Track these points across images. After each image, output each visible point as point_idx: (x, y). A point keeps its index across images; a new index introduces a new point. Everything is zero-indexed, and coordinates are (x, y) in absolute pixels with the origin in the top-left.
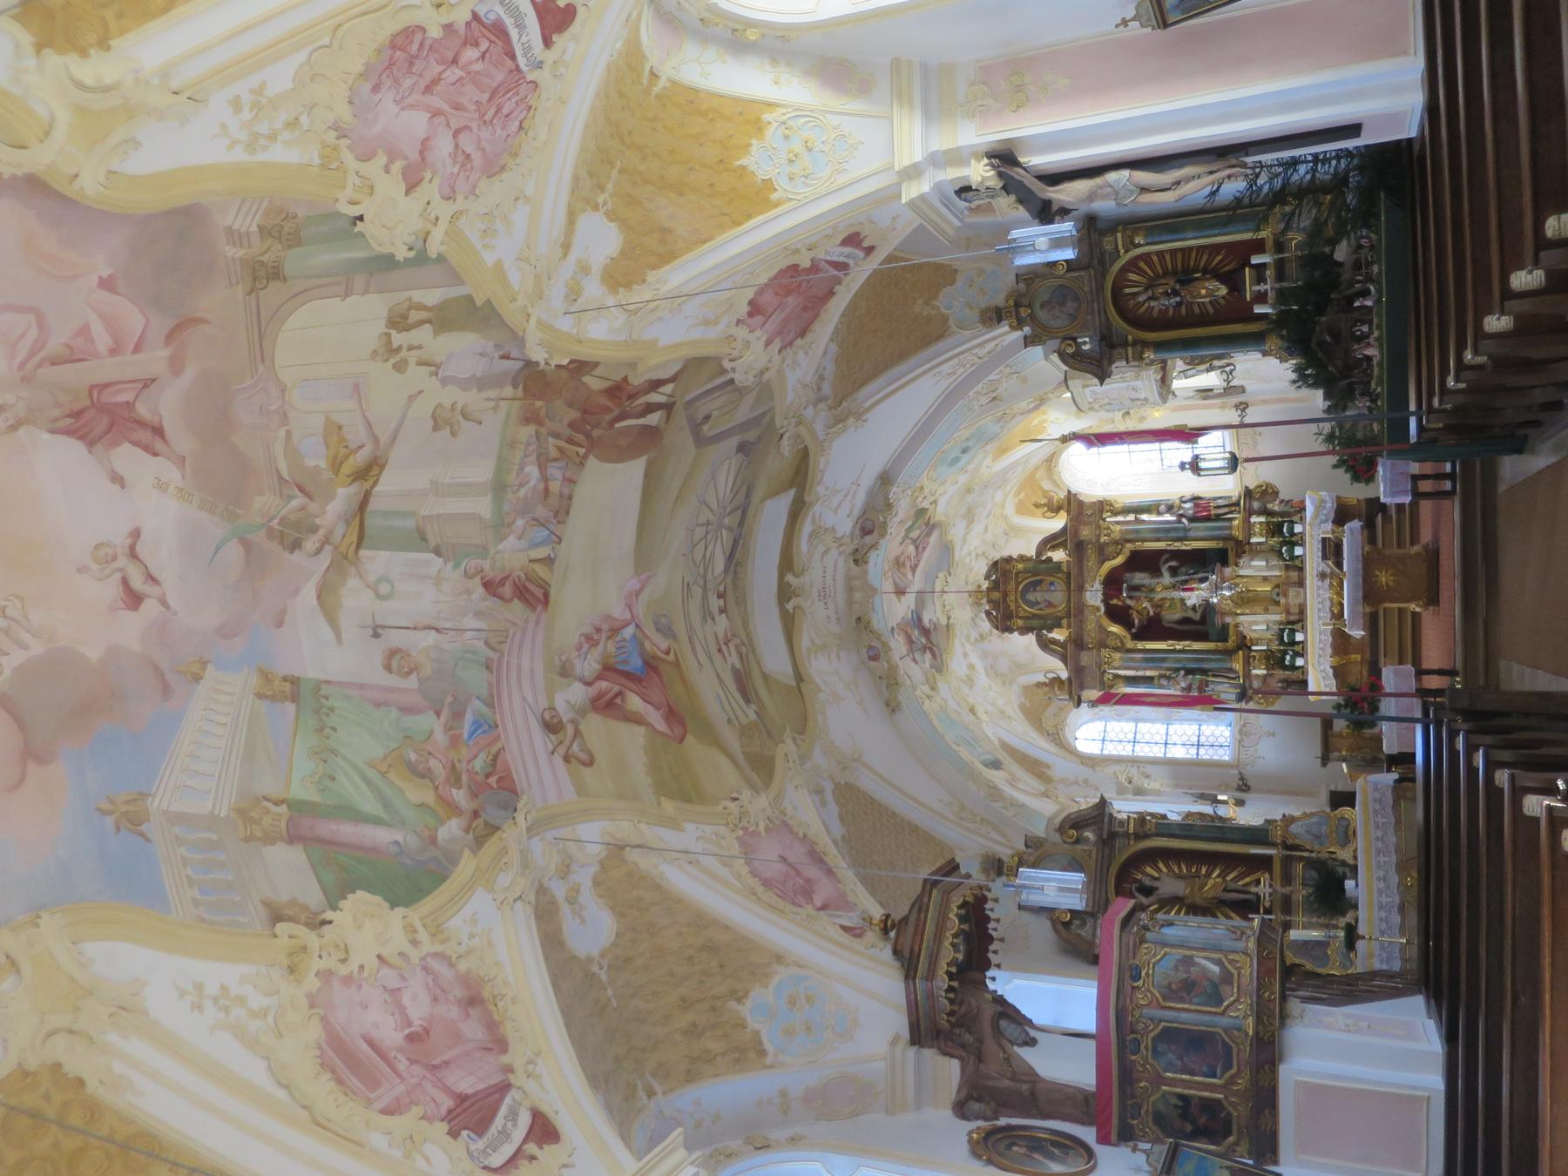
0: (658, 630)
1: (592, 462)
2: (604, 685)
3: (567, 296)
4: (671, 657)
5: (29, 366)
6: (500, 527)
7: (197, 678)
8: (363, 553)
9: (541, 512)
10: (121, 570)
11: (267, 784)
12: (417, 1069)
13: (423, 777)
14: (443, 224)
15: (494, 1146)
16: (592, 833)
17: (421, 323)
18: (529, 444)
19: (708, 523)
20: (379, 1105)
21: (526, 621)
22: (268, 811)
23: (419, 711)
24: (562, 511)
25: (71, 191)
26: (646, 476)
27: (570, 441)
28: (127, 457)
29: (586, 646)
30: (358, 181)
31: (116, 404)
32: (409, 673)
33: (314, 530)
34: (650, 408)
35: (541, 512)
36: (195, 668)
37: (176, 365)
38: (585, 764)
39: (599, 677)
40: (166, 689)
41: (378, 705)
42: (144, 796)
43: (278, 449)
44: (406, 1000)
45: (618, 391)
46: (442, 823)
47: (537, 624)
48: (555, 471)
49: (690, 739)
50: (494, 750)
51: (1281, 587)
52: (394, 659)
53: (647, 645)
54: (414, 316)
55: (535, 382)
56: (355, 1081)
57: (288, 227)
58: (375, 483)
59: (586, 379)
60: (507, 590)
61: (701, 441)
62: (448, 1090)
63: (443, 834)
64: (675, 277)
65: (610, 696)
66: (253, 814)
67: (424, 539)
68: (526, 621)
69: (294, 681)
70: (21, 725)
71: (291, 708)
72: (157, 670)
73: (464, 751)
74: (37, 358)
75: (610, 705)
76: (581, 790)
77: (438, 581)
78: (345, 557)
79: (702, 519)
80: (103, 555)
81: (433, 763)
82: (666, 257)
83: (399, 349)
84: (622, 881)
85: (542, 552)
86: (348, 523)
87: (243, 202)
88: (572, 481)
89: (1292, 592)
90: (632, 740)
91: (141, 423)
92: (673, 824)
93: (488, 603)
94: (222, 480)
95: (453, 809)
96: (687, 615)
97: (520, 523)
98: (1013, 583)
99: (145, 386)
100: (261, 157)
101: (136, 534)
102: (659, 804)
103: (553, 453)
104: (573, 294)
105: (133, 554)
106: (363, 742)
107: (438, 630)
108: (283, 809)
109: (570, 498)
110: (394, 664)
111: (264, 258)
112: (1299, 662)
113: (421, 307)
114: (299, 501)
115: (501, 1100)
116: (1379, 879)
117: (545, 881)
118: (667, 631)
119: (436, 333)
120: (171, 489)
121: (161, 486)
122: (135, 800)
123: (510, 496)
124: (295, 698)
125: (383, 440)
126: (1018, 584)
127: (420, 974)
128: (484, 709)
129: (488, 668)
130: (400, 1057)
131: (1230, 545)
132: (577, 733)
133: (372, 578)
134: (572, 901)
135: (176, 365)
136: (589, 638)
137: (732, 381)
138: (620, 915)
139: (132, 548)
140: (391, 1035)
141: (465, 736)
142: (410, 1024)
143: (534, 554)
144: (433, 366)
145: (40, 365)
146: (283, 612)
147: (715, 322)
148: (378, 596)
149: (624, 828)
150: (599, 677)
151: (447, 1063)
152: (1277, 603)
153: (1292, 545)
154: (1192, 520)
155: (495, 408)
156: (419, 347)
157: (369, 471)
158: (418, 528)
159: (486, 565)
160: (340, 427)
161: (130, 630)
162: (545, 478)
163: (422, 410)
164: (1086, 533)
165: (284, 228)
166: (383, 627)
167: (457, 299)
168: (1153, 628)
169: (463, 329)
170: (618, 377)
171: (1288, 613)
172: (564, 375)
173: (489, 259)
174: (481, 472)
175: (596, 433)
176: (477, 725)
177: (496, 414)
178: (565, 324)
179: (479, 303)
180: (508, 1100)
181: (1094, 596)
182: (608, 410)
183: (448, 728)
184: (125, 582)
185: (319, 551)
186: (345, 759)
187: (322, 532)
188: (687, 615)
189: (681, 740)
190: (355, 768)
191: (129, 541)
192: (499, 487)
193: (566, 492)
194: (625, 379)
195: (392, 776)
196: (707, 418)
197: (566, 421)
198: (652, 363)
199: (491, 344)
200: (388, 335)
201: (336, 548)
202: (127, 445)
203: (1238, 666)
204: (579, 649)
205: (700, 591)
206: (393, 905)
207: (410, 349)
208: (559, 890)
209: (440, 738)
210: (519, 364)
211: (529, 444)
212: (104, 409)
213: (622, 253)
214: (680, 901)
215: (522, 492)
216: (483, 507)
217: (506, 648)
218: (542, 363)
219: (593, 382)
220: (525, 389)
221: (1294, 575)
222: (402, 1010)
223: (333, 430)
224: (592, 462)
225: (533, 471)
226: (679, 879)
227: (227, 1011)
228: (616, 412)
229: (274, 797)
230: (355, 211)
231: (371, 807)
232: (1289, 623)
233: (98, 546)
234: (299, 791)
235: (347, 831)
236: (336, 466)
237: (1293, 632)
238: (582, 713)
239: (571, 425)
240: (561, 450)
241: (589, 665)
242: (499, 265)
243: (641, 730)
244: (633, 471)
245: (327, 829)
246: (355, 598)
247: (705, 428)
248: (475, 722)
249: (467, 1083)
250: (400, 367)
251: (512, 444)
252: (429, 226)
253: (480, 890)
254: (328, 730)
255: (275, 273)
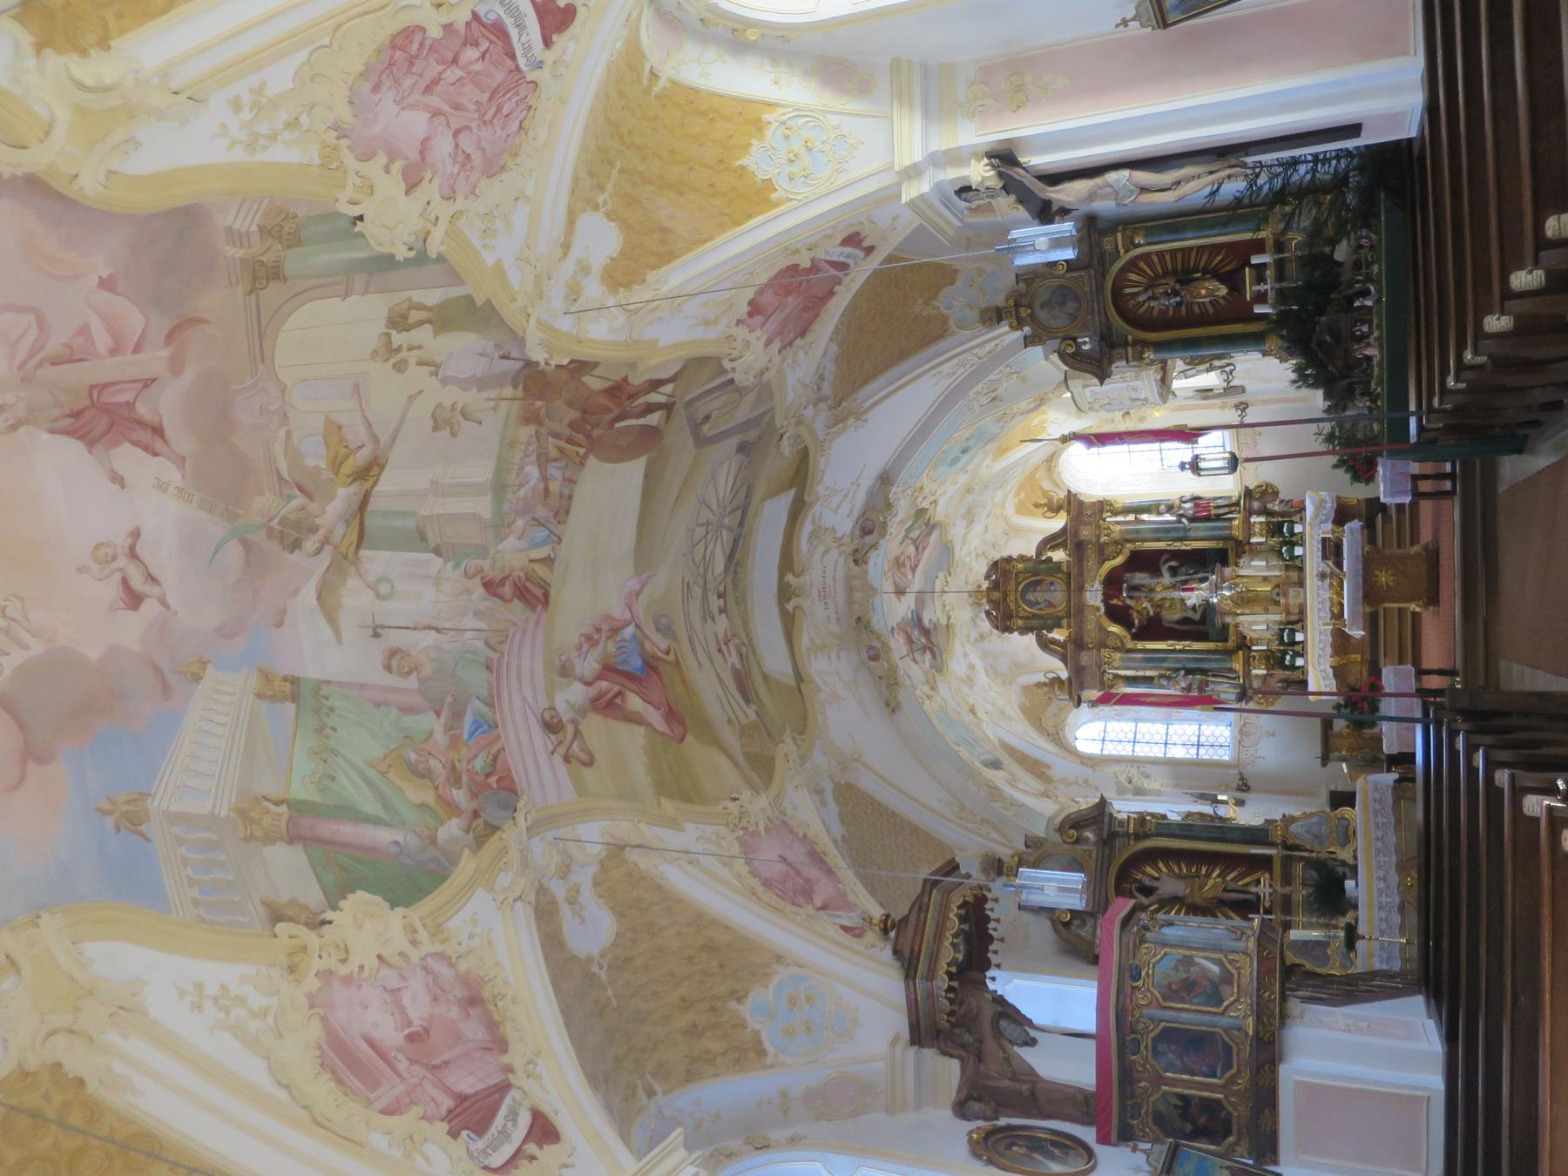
0: (658, 630)
1: (592, 462)
2: (604, 685)
3: (567, 296)
4: (671, 657)
5: (29, 366)
6: (500, 527)
7: (197, 678)
8: (363, 553)
9: (541, 512)
10: (121, 570)
11: (267, 784)
12: (417, 1069)
13: (423, 777)
14: (443, 224)
15: (494, 1146)
16: (592, 833)
17: (421, 323)
18: (529, 444)
19: (708, 523)
20: (379, 1105)
21: (526, 621)
22: (268, 811)
23: (419, 711)
24: (562, 511)
25: (71, 191)
26: (646, 476)
27: (570, 441)
28: (127, 457)
29: (586, 646)
30: (358, 181)
31: (116, 404)
32: (409, 673)
33: (314, 530)
34: (650, 408)
35: (541, 512)
36: (195, 668)
37: (176, 365)
38: (585, 764)
39: (599, 677)
40: (166, 689)
41: (378, 705)
42: (144, 796)
43: (278, 449)
44: (406, 1000)
45: (618, 391)
46: (442, 823)
47: (537, 624)
48: (555, 471)
49: (690, 739)
50: (494, 750)
51: (1281, 587)
52: (394, 659)
53: (647, 645)
54: (414, 316)
55: (535, 382)
56: (355, 1081)
57: (288, 227)
58: (375, 483)
59: (586, 379)
60: (507, 590)
61: (701, 441)
62: (448, 1090)
63: (443, 834)
64: (675, 277)
65: (610, 696)
66: (253, 814)
67: (424, 539)
68: (526, 621)
69: (294, 681)
70: (21, 725)
71: (291, 708)
72: (157, 670)
73: (464, 751)
74: (37, 358)
75: (610, 705)
76: (581, 790)
77: (438, 581)
78: (345, 557)
79: (702, 519)
80: (103, 555)
81: (433, 763)
82: (666, 257)
83: (399, 349)
84: (622, 881)
85: (542, 552)
86: (348, 523)
87: (243, 202)
88: (572, 481)
89: (1292, 592)
90: (632, 740)
91: (141, 423)
92: (673, 824)
93: (488, 603)
94: (222, 480)
95: (453, 809)
96: (687, 615)
97: (520, 523)
98: (1013, 583)
99: (145, 386)
100: (261, 157)
101: (136, 534)
102: (659, 804)
103: (553, 453)
104: (573, 294)
105: (133, 554)
106: (363, 742)
107: (438, 630)
108: (283, 809)
109: (570, 498)
110: (394, 664)
111: (264, 258)
112: (1299, 662)
113: (421, 307)
114: (299, 501)
115: (501, 1100)
116: (1379, 879)
117: (545, 881)
118: (667, 631)
119: (436, 333)
120: (171, 489)
121: (161, 486)
122: (135, 800)
123: (510, 496)
124: (295, 698)
125: (383, 440)
126: (1018, 584)
127: (420, 974)
128: (484, 709)
129: (488, 668)
130: (400, 1057)
131: (1230, 545)
132: (577, 733)
133: (372, 578)
134: (572, 901)
135: (176, 365)
136: (589, 638)
137: (732, 381)
138: (620, 915)
139: (132, 548)
140: (391, 1035)
141: (465, 736)
142: (410, 1024)
143: (534, 554)
144: (433, 366)
145: (40, 365)
146: (283, 612)
147: (715, 322)
148: (378, 596)
149: (624, 828)
150: (599, 677)
151: (447, 1063)
152: (1277, 603)
153: (1292, 545)
154: (1192, 520)
155: (495, 408)
156: (419, 347)
157: (369, 471)
158: (418, 528)
159: (486, 565)
160: (340, 427)
161: (130, 630)
162: (545, 478)
163: (422, 410)
164: (1086, 533)
165: (284, 228)
166: (383, 627)
167: (457, 299)
168: (1153, 628)
169: (463, 329)
170: (618, 377)
171: (1288, 613)
172: (564, 375)
173: (489, 259)
174: (481, 472)
175: (596, 433)
176: (477, 725)
177: (496, 414)
178: (565, 324)
179: (479, 303)
180: (508, 1100)
181: (1094, 596)
182: (608, 410)
183: (448, 728)
184: (125, 582)
185: (319, 551)
186: (345, 759)
187: (322, 532)
188: (687, 615)
189: (681, 740)
190: (355, 768)
191: (129, 541)
192: (499, 487)
193: (566, 492)
194: (625, 379)
195: (392, 776)
196: (707, 418)
197: (566, 421)
198: (652, 363)
199: (491, 344)
200: (388, 335)
201: (336, 548)
202: (127, 445)
203: (1238, 666)
204: (579, 649)
205: (700, 591)
206: (393, 905)
207: (410, 349)
208: (559, 890)
209: (440, 738)
210: (519, 364)
211: (529, 444)
212: (104, 409)
213: (622, 253)
214: (680, 901)
215: (522, 492)
216: (483, 507)
217: (506, 648)
218: (542, 363)
219: (593, 382)
220: (525, 389)
221: (1294, 575)
222: (402, 1010)
223: (333, 430)
224: (592, 462)
225: (533, 471)
226: (679, 879)
227: (227, 1011)
228: (616, 412)
229: (274, 797)
230: (355, 211)
231: (371, 807)
232: (1289, 623)
233: (98, 546)
234: (299, 791)
235: (347, 831)
236: (336, 466)
237: (1293, 632)
238: (582, 713)
239: (571, 425)
240: (561, 450)
241: (589, 665)
242: (499, 265)
243: (641, 730)
244: (633, 471)
245: (327, 829)
246: (355, 598)
247: (705, 428)
248: (475, 722)
249: (467, 1083)
250: (400, 367)
251: (512, 444)
252: (429, 226)
253: (480, 890)
254: (328, 730)
255: (275, 273)
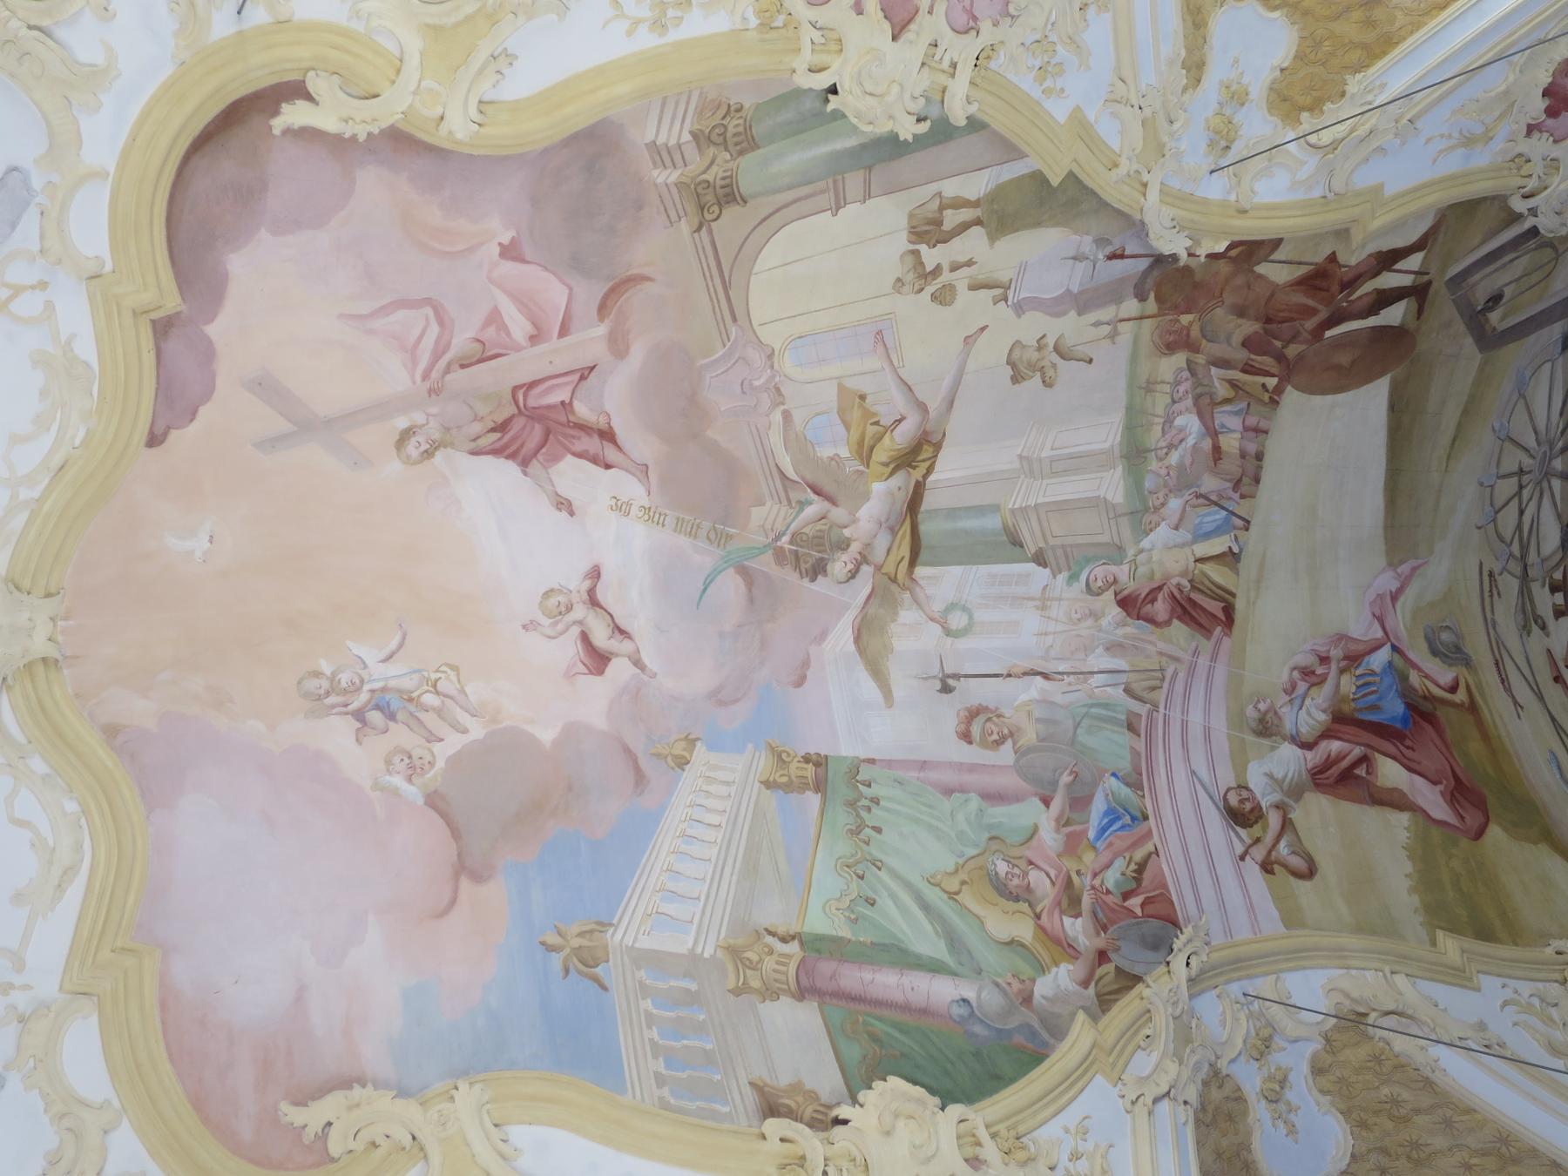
0: (1435, 652)
1: (1291, 396)
2: (1335, 746)
3: (1212, 144)
4: (1461, 696)
5: (435, 375)
6: (1142, 514)
7: (682, 762)
8: (921, 571)
9: (1210, 484)
10: (580, 623)
11: (774, 912)
13: (1017, 899)
14: (965, 73)
16: (1312, 989)
17: (964, 227)
18: (1177, 383)
19: (1521, 472)
21: (1196, 653)
22: (771, 952)
23: (1017, 798)
24: (1248, 476)
25: (439, 138)
26: (1392, 407)
27: (1248, 369)
28: (571, 474)
29: (1302, 687)
30: (817, 36)
31: (550, 407)
32: (999, 743)
33: (844, 545)
34: (1385, 299)
35: (1210, 484)
36: (679, 749)
37: (618, 345)
38: (1296, 874)
39: (1327, 734)
40: (640, 778)
41: (948, 791)
42: (604, 925)
43: (776, 439)
45: (1324, 279)
46: (1043, 970)
47: (1214, 657)
48: (1229, 419)
49: (1495, 832)
50: (1139, 855)
52: (976, 724)
53: (1414, 679)
54: (951, 219)
55: (1172, 286)
57: (733, 125)
58: (929, 471)
59: (1261, 269)
60: (1161, 608)
61: (1489, 340)
63: (1043, 988)
64: (1396, 75)
65: (1345, 764)
66: (749, 955)
67: (1017, 542)
68: (1196, 653)
69: (819, 761)
70: (456, 833)
71: (814, 799)
72: (627, 751)
73: (1088, 857)
74: (442, 363)
75: (1347, 777)
76: (1292, 918)
77: (1043, 603)
78: (894, 580)
79: (1510, 465)
80: (555, 606)
81: (1035, 877)
82: (1379, 46)
83: (937, 270)
84: (1366, 1070)
85: (1218, 545)
86: (893, 531)
87: (664, 104)
88: (1260, 431)
90: (1385, 840)
91: (583, 428)
92: (1459, 977)
93: (1128, 630)
94: (703, 492)
95: (1065, 948)
96: (1490, 625)
97: (1175, 504)
99: (583, 378)
100: (674, 36)
101: (595, 574)
102: (1434, 943)
103: (1222, 391)
104: (1222, 139)
105: (593, 601)
106: (922, 848)
107: (1045, 676)
108: (793, 948)
109: (1259, 457)
110: (976, 729)
111: (709, 177)
113: (959, 203)
114: (817, 506)
117: (1222, 1064)
118: (1454, 654)
119: (992, 239)
120: (634, 510)
121: (621, 507)
122: (591, 932)
123: (1154, 465)
124: (820, 786)
125: (934, 406)
128: (1125, 791)
129: (1131, 728)
132: (1286, 824)
133: (937, 607)
134: (1273, 1098)
135: (618, 345)
136: (1307, 673)
137: (1534, 232)
138: (1360, 1125)
139: (591, 593)
141: (1091, 834)
143: (1203, 549)
144: (1000, 289)
145: (448, 370)
146: (806, 664)
147: (1488, 138)
148: (948, 632)
149: (1368, 983)
150: (1327, 734)
155: (1113, 336)
156: (970, 263)
157: (919, 453)
158: (1005, 528)
159: (1122, 572)
160: (863, 397)
161: (594, 701)
162: (1213, 433)
163: (991, 354)
165: (729, 129)
166: (957, 677)
167: (1017, 182)
169: (1038, 224)
170: (1319, 257)
172: (1224, 267)
173: (1059, 111)
174: (1105, 434)
175: (1292, 351)
176: (1112, 815)
177: (1115, 350)
178: (1215, 189)
179: (1055, 182)
182: (1310, 312)
183: (1062, 822)
184: (585, 638)
185: (853, 575)
186: (894, 874)
187: (855, 547)
188: (1490, 625)
189: (1479, 834)
190: (908, 886)
191: (588, 584)
192: (1134, 454)
193: (1252, 448)
194: (1332, 258)
195: (966, 898)
196: (1496, 299)
197: (1237, 338)
198: (1376, 224)
199: (1088, 239)
200: (916, 253)
201: (878, 568)
202: (570, 458)
204: (1291, 689)
205: (1514, 584)
206: (947, 1098)
207: (955, 267)
208: (1250, 1078)
209: (1050, 838)
210: (1143, 264)
211: (1177, 383)
212: (535, 415)
213: (1300, 57)
214: (1470, 1111)
215: (1174, 458)
216: (1112, 486)
217: (1160, 696)
218: (1183, 255)
219: (1276, 273)
220: (1158, 299)
223: (853, 402)
224: (1291, 396)
225: (1190, 423)
226: (1465, 1075)
228: (1324, 313)
229: (781, 930)
230: (822, 81)
231: (929, 944)
233: (547, 594)
234: (818, 922)
235: (886, 982)
236: (864, 452)
238: (1296, 792)
239: (1246, 344)
240: (1233, 384)
241: (1311, 715)
242: (1077, 117)
243: (1404, 818)
244: (1373, 399)
245: (855, 978)
246: (912, 637)
247: (1494, 317)
248: (1106, 814)
250: (944, 297)
251: (1150, 387)
252: (943, 79)
253: (1099, 1080)
254: (868, 831)
255: (729, 195)
